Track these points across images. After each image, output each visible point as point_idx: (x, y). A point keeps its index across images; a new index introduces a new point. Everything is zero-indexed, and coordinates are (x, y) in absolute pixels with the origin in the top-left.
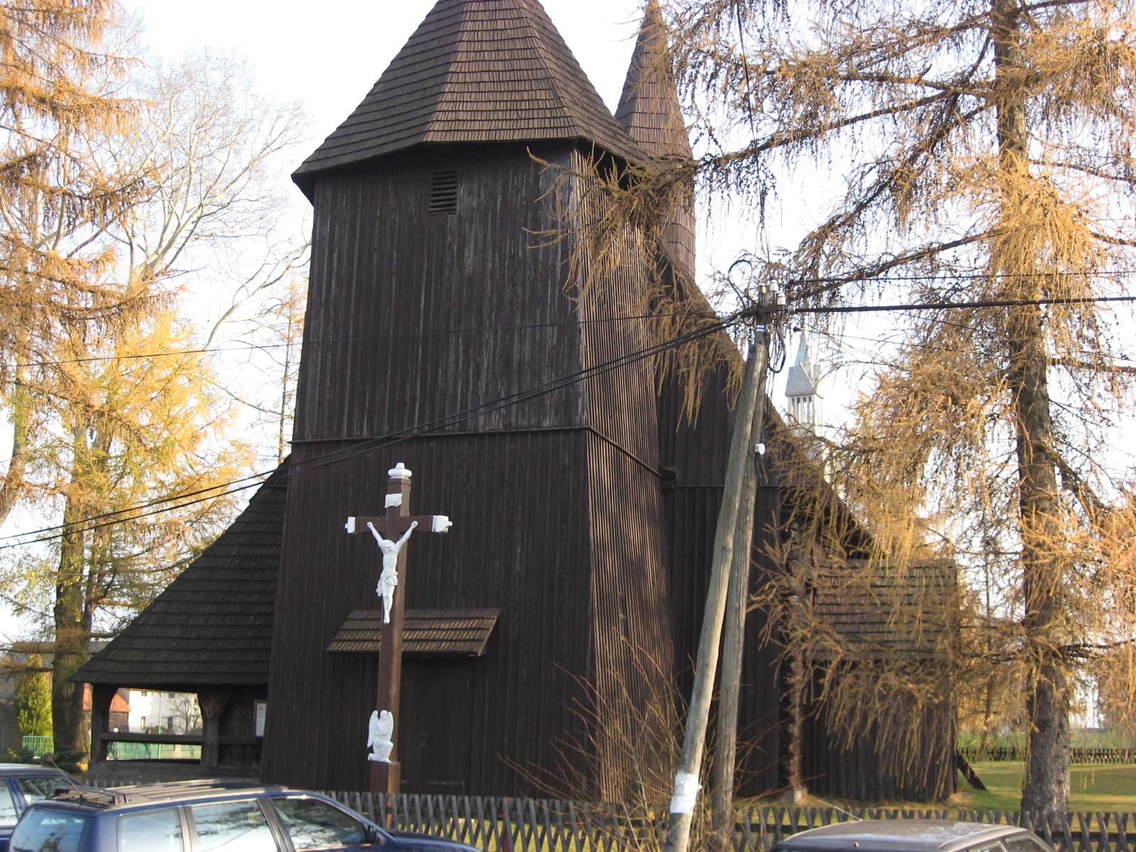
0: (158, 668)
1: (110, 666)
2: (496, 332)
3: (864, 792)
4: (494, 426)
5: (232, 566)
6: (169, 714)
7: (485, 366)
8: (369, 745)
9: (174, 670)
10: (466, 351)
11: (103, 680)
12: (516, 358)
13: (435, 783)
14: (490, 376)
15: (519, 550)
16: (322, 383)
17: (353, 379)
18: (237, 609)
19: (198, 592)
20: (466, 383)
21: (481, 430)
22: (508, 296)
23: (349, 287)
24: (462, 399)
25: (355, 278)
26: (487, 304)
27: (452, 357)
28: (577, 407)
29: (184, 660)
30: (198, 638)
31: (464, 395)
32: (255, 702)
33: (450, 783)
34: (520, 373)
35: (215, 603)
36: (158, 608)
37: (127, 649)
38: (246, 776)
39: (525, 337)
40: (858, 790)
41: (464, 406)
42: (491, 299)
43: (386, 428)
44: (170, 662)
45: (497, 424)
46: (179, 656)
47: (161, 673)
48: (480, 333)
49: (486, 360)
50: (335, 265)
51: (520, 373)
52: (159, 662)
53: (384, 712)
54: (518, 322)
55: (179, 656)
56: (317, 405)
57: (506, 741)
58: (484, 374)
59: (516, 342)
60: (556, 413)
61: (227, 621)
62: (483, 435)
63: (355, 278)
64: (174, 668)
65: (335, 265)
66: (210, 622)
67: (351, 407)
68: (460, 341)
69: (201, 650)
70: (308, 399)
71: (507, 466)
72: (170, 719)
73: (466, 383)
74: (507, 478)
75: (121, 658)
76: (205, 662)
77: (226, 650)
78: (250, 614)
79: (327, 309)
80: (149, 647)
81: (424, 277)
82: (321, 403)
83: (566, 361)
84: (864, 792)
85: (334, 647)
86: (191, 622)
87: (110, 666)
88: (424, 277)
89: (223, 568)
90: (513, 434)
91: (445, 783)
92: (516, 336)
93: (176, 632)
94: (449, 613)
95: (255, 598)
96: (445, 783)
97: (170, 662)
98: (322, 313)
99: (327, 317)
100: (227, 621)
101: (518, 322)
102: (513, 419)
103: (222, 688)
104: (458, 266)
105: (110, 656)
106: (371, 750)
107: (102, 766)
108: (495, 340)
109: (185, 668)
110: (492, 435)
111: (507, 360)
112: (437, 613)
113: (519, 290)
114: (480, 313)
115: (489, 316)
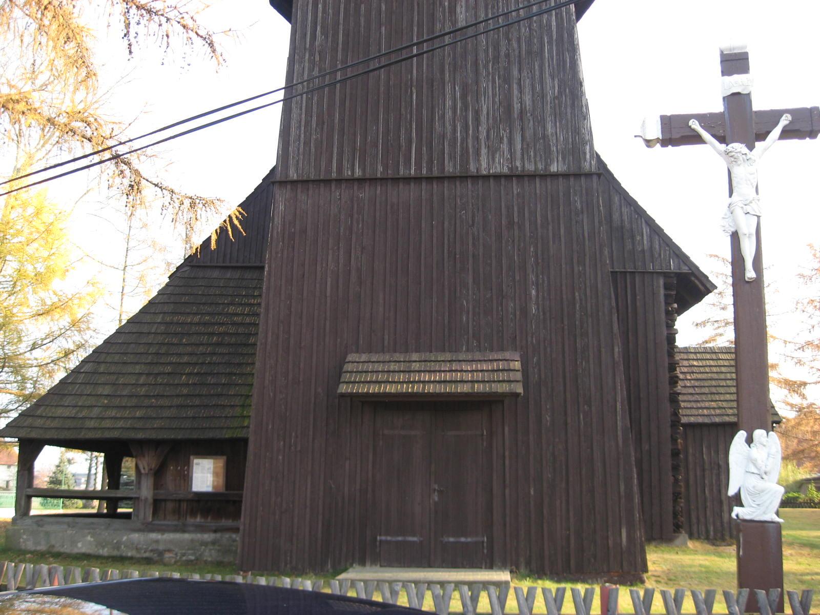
0: (91, 424)
1: (39, 422)
2: (494, 82)
3: (712, 533)
4: (498, 170)
5: (159, 331)
6: (7, 478)
7: (485, 112)
8: (731, 492)
9: (108, 426)
10: (464, 96)
11: (34, 435)
12: (517, 106)
13: (452, 539)
14: (491, 121)
15: (534, 292)
16: (308, 123)
17: (342, 120)
18: (169, 369)
19: (125, 354)
20: (466, 127)
21: (484, 173)
22: (503, 50)
23: (336, 34)
24: (462, 143)
25: (341, 27)
26: (482, 55)
27: (449, 103)
28: (585, 154)
29: (118, 415)
30: (131, 396)
31: (465, 140)
32: (192, 457)
33: (469, 540)
34: (521, 119)
35: (145, 364)
36: (86, 368)
37: (57, 406)
38: (184, 531)
39: (525, 86)
40: (707, 532)
41: (465, 151)
42: (486, 51)
43: (380, 168)
44: (103, 419)
45: (500, 167)
46: (113, 413)
47: (95, 428)
48: (477, 83)
49: (485, 108)
50: (320, 14)
51: (521, 119)
52: (92, 418)
53: (759, 434)
54: (515, 72)
55: (113, 413)
56: (302, 145)
57: (532, 492)
58: (483, 119)
59: (516, 92)
60: (564, 159)
61: (159, 380)
62: (487, 177)
63: (341, 27)
64: (107, 424)
65: (320, 14)
66: (141, 381)
67: (341, 146)
68: (457, 88)
69: (135, 407)
70: (292, 139)
71: (516, 209)
72: (8, 482)
73: (466, 127)
74: (516, 220)
75: (50, 415)
76: (140, 418)
77: (161, 407)
78: (182, 374)
79: (312, 54)
80: (80, 404)
81: (415, 29)
82: (307, 143)
83: (569, 110)
84: (712, 533)
85: (343, 389)
86: (121, 381)
87: (39, 422)
88: (415, 29)
89: (149, 333)
90: (520, 177)
91: (463, 539)
92: (515, 86)
93: (107, 390)
94: (462, 356)
95: (185, 359)
96: (463, 539)
97: (103, 419)
98: (307, 57)
99: (312, 62)
100: (159, 380)
101: (515, 72)
102: (518, 164)
103: (156, 444)
104: (451, 20)
105: (39, 412)
106: (737, 500)
107: (28, 521)
108: (494, 88)
109: (121, 424)
110: (497, 177)
111: (509, 109)
112: (448, 356)
113: (515, 45)
114: (476, 63)
115: (486, 67)
